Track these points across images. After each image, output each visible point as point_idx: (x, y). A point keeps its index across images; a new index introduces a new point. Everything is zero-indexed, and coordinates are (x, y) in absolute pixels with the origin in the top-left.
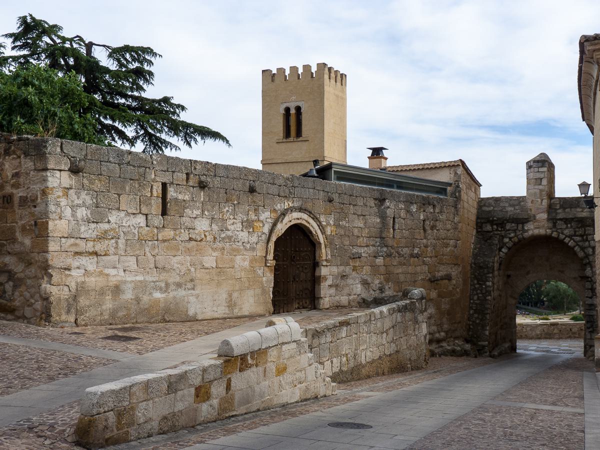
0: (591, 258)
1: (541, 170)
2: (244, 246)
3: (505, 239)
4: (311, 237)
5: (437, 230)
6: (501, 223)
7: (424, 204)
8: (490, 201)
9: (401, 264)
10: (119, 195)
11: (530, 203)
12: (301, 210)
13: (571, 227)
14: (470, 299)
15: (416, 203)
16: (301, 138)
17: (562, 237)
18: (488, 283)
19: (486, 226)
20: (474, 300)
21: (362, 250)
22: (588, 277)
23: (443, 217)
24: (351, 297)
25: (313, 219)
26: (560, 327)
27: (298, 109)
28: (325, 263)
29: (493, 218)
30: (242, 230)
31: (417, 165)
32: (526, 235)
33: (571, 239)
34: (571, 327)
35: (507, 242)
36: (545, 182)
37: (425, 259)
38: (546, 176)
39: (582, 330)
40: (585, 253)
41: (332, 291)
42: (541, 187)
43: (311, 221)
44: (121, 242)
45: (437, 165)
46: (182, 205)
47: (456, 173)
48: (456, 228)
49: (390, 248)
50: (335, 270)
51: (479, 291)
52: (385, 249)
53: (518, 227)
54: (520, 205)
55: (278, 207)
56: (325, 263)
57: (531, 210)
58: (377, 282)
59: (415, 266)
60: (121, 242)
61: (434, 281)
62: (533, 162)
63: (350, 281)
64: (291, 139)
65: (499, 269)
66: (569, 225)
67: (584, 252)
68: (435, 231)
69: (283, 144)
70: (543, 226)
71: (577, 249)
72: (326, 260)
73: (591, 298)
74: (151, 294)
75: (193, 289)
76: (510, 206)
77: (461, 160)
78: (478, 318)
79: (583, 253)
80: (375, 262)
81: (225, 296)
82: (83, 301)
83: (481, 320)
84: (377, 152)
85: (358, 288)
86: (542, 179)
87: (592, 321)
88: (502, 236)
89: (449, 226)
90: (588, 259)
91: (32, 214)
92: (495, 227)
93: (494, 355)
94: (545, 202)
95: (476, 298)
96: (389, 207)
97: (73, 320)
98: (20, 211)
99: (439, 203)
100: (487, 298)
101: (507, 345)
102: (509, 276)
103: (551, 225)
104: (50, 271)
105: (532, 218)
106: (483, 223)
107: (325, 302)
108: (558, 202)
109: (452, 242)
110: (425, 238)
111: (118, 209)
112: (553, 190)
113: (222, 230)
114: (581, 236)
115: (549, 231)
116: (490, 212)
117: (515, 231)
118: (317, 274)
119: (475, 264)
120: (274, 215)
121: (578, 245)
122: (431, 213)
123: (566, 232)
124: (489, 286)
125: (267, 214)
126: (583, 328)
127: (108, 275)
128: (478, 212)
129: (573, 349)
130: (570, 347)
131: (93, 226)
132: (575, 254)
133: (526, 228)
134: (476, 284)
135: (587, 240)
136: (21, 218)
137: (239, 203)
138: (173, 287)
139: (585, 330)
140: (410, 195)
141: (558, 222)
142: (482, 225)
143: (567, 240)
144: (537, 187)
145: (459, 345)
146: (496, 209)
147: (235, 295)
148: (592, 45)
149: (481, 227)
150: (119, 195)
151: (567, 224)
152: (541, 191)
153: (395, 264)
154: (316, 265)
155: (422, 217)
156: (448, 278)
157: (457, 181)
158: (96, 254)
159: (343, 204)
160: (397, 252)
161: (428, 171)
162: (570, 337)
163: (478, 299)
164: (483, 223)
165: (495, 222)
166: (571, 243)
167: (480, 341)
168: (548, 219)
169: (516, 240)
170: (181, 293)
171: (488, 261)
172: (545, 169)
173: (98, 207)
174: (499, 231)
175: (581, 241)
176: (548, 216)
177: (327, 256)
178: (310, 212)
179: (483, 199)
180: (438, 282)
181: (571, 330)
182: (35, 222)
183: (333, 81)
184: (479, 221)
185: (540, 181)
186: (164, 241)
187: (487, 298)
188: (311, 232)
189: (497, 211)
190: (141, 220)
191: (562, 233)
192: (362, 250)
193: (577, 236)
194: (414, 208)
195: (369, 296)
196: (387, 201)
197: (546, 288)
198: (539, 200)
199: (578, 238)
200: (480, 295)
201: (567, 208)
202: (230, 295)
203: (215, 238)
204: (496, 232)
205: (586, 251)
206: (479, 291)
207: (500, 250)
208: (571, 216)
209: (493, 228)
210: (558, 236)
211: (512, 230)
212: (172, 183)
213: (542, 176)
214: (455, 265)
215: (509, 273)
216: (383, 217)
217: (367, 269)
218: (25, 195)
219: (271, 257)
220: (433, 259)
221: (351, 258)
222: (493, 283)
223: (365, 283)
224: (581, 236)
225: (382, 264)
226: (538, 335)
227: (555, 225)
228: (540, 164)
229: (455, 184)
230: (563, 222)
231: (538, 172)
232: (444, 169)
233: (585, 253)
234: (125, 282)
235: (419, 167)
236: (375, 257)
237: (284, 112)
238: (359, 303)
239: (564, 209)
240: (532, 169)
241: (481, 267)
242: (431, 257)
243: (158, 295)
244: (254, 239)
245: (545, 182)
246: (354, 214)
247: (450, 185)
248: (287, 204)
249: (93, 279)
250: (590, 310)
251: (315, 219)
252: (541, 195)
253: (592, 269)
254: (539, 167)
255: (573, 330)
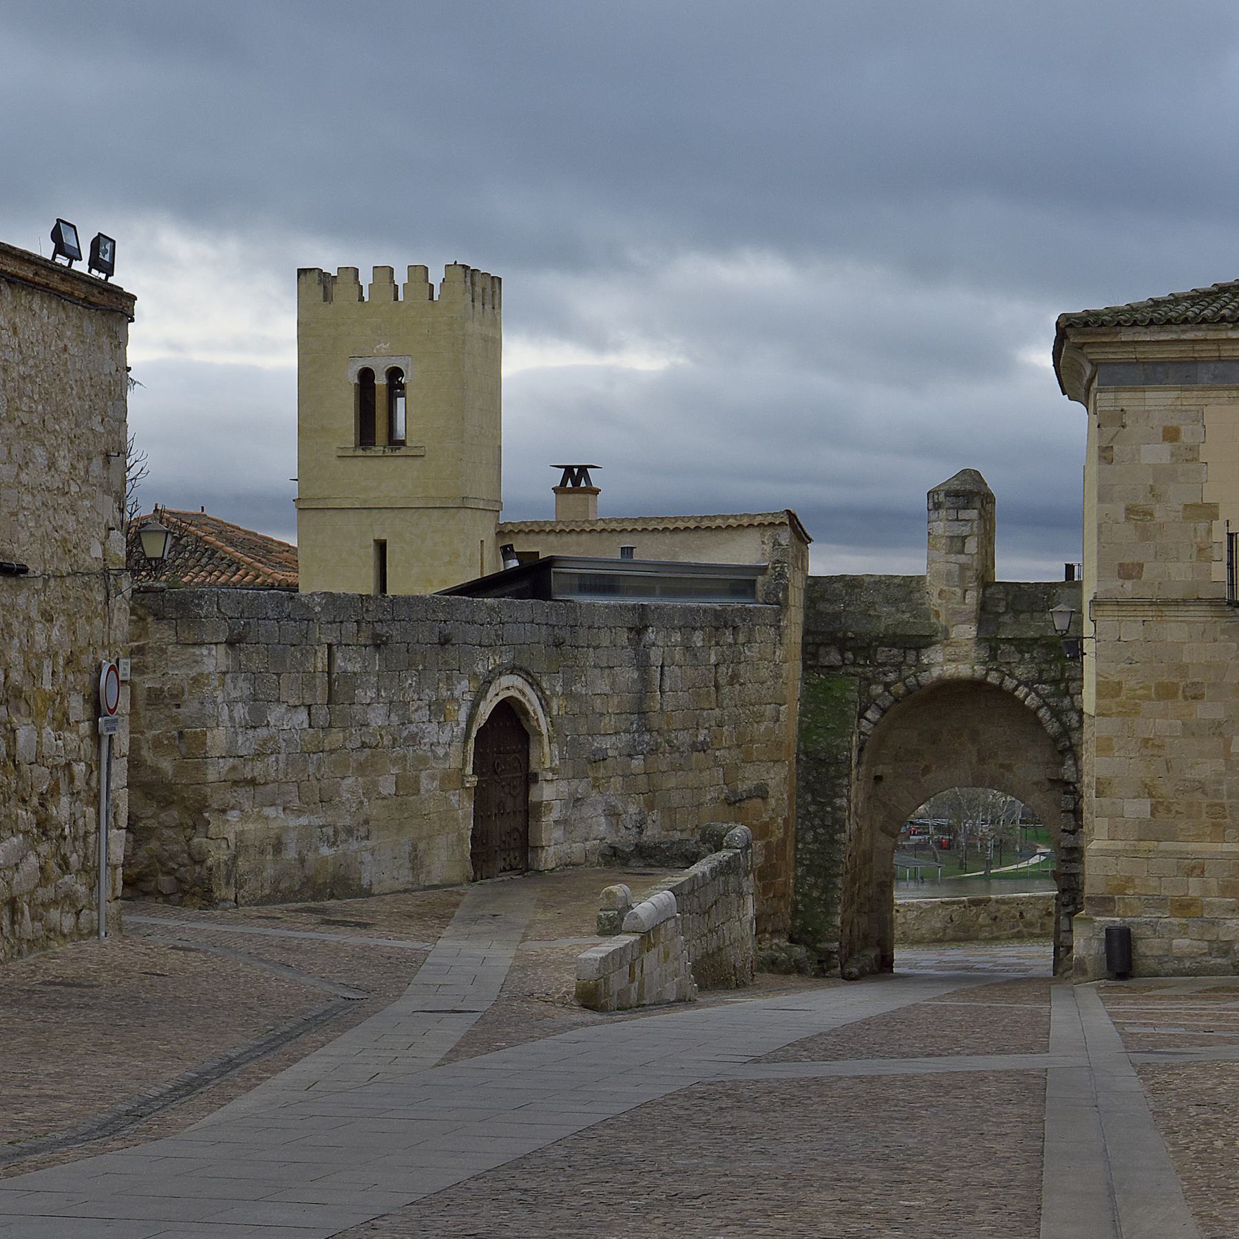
0: (1075, 736)
1: (963, 515)
2: (432, 751)
3: (874, 687)
4: (524, 723)
5: (741, 685)
6: (864, 647)
7: (717, 629)
8: (836, 585)
9: (675, 768)
10: (278, 675)
11: (936, 594)
12: (513, 670)
13: (1032, 658)
14: (797, 841)
15: (702, 628)
16: (403, 448)
17: (1009, 683)
18: (838, 801)
19: (828, 653)
20: (806, 843)
21: (606, 743)
22: (1068, 783)
23: (752, 652)
24: (588, 845)
25: (531, 685)
26: (992, 909)
27: (394, 374)
28: (549, 776)
29: (845, 633)
30: (430, 721)
31: (683, 519)
32: (925, 678)
33: (1031, 689)
34: (1023, 907)
35: (879, 696)
36: (972, 546)
37: (718, 753)
38: (975, 529)
39: (1049, 914)
40: (1062, 724)
41: (558, 833)
42: (962, 559)
43: (528, 690)
44: (282, 757)
45: (731, 521)
46: (351, 680)
47: (776, 544)
48: (777, 676)
49: (655, 734)
50: (563, 787)
51: (817, 822)
52: (647, 737)
53: (905, 657)
54: (911, 600)
55: (480, 669)
56: (549, 776)
57: (937, 614)
58: (633, 809)
59: (700, 771)
60: (282, 757)
61: (735, 802)
62: (946, 495)
63: (587, 811)
64: (378, 450)
65: (859, 764)
66: (1027, 656)
67: (1059, 720)
68: (737, 686)
69: (356, 460)
70: (966, 657)
71: (1043, 713)
72: (552, 770)
73: (1073, 832)
74: (317, 849)
75: (367, 838)
76: (887, 601)
77: (788, 511)
78: (815, 885)
79: (1057, 725)
80: (629, 766)
81: (408, 849)
82: (243, 865)
83: (825, 890)
84: (575, 478)
85: (601, 826)
86: (966, 537)
87: (1073, 889)
88: (867, 679)
89: (764, 673)
90: (1070, 739)
91: (175, 720)
92: (850, 655)
93: (850, 973)
94: (972, 598)
95: (810, 836)
96: (654, 644)
97: (233, 897)
98: (149, 714)
99: (745, 620)
100: (838, 836)
101: (873, 953)
102: (878, 779)
103: (984, 654)
104: (206, 815)
105: (940, 637)
106: (819, 645)
107: (548, 858)
108: (1001, 596)
109: (769, 710)
110: (719, 705)
111: (278, 700)
112: (989, 563)
113: (403, 724)
114: (1054, 682)
115: (979, 670)
116: (836, 616)
117: (898, 667)
118: (534, 797)
119: (806, 754)
120: (474, 686)
121: (1047, 704)
122: (730, 645)
123: (1020, 671)
124: (841, 808)
125: (465, 683)
126: (1053, 909)
127: (267, 818)
128: (806, 616)
129: (1027, 962)
130: (1019, 958)
131: (250, 732)
132: (1039, 723)
133: (925, 661)
134: (809, 804)
135: (1067, 692)
136: (151, 726)
137: (425, 669)
138: (343, 836)
139: (1058, 911)
140: (691, 610)
141: (1002, 647)
142: (817, 651)
143: (1021, 692)
144: (953, 558)
145: (782, 949)
146: (851, 609)
147: (422, 846)
148: (1081, 334)
149: (815, 656)
150: (278, 675)
151: (1021, 652)
152: (963, 568)
153: (664, 768)
154: (530, 779)
155: (713, 660)
156: (761, 792)
157: (778, 562)
158: (253, 782)
159: (577, 647)
160: (669, 742)
161: (708, 534)
162: (1019, 936)
163: (815, 840)
164: (819, 645)
165: (849, 644)
166: (1031, 701)
167: (820, 941)
168: (979, 640)
169: (900, 688)
170: (354, 845)
171: (837, 746)
172: (973, 514)
173: (255, 700)
174: (861, 666)
175: (1053, 695)
176: (979, 630)
177: (552, 761)
178: (528, 674)
179: (817, 580)
180: (743, 805)
181: (1021, 914)
182: (181, 733)
183: (478, 304)
184: (810, 639)
185: (959, 544)
186: (332, 751)
187: (838, 836)
188: (526, 713)
189: (853, 613)
190: (302, 715)
191: (1011, 675)
192: (606, 743)
193: (1045, 682)
194: (698, 639)
195: (625, 838)
196: (650, 629)
197: (36, 274)
198: (959, 591)
199: (1045, 689)
200: (821, 831)
201: (1022, 612)
202: (415, 848)
203: (395, 739)
204: (851, 670)
205: (1065, 719)
206: (817, 822)
207: (861, 716)
208: (1031, 634)
209: (843, 659)
210: (1001, 683)
211: (893, 665)
212: (340, 644)
213: (965, 530)
214: (775, 762)
215: (879, 770)
216: (643, 665)
217: (617, 782)
218: (158, 686)
219: (469, 770)
220: (733, 753)
221: (590, 762)
222: (849, 801)
223: (613, 814)
224: (1054, 682)
225: (641, 769)
226: (935, 933)
227: (993, 657)
228: (962, 501)
229: (774, 568)
230: (1013, 648)
231: (957, 520)
232: (748, 530)
233: (1062, 724)
234: (286, 829)
235: (688, 525)
236: (630, 755)
237: (356, 381)
238: (603, 855)
239: (1017, 613)
240: (943, 513)
241: (821, 762)
242: (729, 748)
243: (325, 851)
244: (445, 737)
245: (972, 546)
246: (595, 667)
247: (763, 570)
248: (493, 661)
249: (251, 826)
250: (1070, 861)
251: (535, 684)
252: (962, 577)
253: (1076, 764)
254: (958, 509)
255: (1028, 916)
